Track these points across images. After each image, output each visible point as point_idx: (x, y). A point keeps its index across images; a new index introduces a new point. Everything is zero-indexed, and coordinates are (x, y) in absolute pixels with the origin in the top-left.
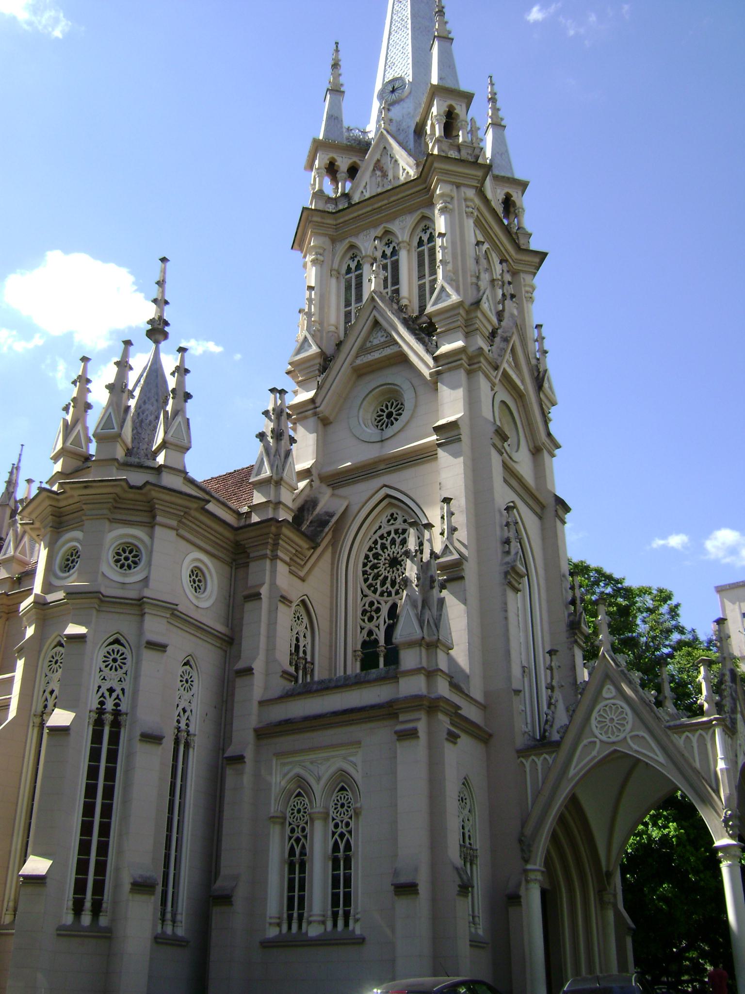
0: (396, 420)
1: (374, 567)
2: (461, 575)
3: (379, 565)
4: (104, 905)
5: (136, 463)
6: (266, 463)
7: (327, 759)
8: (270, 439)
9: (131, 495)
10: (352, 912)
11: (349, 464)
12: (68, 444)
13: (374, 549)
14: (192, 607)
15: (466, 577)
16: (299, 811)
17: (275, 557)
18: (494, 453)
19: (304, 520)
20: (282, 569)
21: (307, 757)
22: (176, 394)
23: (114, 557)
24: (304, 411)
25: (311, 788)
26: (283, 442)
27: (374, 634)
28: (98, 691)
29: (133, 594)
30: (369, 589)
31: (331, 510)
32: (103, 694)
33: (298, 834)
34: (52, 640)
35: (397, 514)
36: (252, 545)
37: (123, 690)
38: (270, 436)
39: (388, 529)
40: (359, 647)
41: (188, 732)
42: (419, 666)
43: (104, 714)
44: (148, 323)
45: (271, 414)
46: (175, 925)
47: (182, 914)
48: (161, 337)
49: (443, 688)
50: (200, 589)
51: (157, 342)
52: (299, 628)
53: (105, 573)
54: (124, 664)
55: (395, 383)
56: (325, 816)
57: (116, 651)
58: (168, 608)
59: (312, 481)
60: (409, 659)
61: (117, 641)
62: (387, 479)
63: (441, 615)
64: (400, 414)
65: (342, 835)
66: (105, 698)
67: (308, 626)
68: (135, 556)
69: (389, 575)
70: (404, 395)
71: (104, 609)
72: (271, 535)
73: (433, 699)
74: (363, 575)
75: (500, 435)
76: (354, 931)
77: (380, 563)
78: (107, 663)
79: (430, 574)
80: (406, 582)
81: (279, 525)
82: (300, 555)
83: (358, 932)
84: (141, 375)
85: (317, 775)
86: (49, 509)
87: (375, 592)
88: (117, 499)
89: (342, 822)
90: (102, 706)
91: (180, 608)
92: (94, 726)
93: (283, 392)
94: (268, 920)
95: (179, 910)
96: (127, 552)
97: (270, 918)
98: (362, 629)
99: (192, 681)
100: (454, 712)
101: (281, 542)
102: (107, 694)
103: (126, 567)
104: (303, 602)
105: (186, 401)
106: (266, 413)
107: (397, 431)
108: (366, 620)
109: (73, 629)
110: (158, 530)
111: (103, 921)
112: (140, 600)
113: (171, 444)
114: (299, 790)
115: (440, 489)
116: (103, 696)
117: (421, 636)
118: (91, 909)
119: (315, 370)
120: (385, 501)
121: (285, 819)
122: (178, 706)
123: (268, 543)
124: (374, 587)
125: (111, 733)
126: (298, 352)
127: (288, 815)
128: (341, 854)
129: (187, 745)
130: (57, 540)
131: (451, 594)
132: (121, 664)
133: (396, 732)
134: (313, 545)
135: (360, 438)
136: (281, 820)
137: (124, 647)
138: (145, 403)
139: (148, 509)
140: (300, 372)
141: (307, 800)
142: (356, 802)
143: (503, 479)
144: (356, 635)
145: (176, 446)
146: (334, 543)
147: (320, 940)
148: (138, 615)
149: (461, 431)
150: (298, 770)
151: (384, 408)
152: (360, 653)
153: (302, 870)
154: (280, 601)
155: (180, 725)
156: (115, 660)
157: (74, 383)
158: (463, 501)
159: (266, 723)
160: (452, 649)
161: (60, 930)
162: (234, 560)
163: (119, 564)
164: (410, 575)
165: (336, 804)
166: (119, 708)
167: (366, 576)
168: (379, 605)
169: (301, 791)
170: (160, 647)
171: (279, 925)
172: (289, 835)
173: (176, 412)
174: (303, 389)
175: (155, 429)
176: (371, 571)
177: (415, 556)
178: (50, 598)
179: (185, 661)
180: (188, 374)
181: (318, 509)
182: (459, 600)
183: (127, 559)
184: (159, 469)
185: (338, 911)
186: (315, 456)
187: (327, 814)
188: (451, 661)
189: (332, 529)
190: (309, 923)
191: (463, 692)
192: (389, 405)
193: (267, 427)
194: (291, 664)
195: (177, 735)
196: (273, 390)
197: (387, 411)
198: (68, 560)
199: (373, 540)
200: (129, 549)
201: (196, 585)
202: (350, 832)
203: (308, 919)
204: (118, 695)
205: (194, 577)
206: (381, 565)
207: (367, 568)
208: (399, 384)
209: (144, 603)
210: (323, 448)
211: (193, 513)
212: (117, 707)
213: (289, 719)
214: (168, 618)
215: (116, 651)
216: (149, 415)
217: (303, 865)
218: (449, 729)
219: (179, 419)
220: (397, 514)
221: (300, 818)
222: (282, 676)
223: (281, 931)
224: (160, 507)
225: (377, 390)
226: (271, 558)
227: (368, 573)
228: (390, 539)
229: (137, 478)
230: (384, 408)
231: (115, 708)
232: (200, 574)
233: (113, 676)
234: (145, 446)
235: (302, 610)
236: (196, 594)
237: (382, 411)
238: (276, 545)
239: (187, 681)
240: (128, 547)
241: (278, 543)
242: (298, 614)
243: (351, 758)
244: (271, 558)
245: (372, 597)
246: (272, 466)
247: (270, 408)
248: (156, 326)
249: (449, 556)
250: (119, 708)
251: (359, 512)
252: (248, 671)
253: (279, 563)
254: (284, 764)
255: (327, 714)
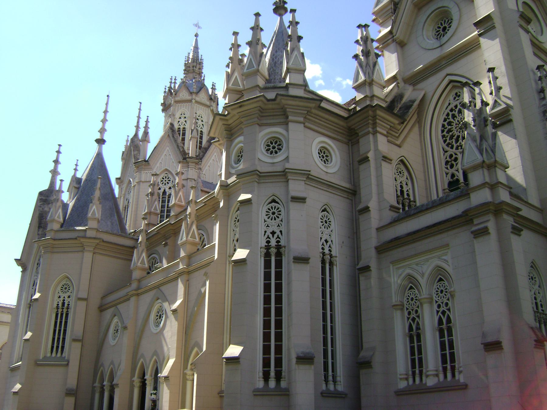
0: (448, 30)
1: (448, 132)
2: (509, 118)
3: (452, 129)
4: (283, 374)
5: (272, 87)
6: (361, 72)
7: (427, 260)
8: (361, 57)
9: (270, 106)
10: (457, 366)
11: (422, 66)
12: (230, 85)
13: (447, 119)
14: (323, 173)
15: (514, 119)
16: (412, 299)
17: (375, 133)
18: (522, 32)
19: (395, 108)
20: (382, 140)
21: (413, 261)
22: (292, 39)
23: (266, 148)
24: (385, 42)
25: (418, 282)
26: (371, 57)
27: (456, 176)
28: (265, 234)
29: (279, 168)
30: (448, 147)
31: (413, 98)
32: (268, 236)
33: (413, 315)
34: (235, 206)
35: (460, 92)
36: (358, 127)
37: (281, 232)
38: (361, 55)
39: (455, 104)
40: (446, 187)
41: (331, 256)
42: (484, 182)
43: (270, 249)
44: (273, 5)
45: (360, 41)
46: (336, 384)
47: (340, 376)
48: (282, 12)
49: (504, 196)
50: (328, 161)
51: (281, 15)
52: (401, 179)
53: (260, 158)
54: (280, 215)
55: (444, 5)
56: (430, 300)
57: (273, 207)
58: (304, 174)
59: (398, 83)
60: (476, 179)
61: (274, 201)
62: (448, 70)
63: (495, 144)
64: (450, 27)
65: (443, 313)
66: (270, 238)
67: (408, 177)
68: (280, 145)
69: (460, 134)
70: (452, 12)
71: (262, 181)
72: (370, 118)
73: (497, 204)
74: (443, 138)
75: (524, 18)
76: (459, 380)
77: (453, 128)
78: (271, 218)
79: (483, 116)
80: (466, 125)
81: (374, 109)
82: (394, 130)
83: (462, 380)
84: (273, 37)
85: (421, 273)
86: (223, 127)
87: (452, 148)
88: (261, 110)
89: (442, 303)
90: (268, 244)
91: (312, 173)
92: (264, 258)
93: (366, 26)
94: (399, 376)
95: (338, 374)
96: (274, 143)
97: (400, 375)
98: (447, 174)
99: (330, 222)
100: (515, 212)
101: (378, 121)
102: (271, 236)
103: (274, 153)
104: (402, 161)
105: (299, 41)
106: (357, 42)
107: (450, 37)
108: (449, 168)
109: (244, 197)
110: (291, 125)
111: (283, 384)
112: (283, 172)
113: (292, 69)
114: (411, 285)
115: (485, 64)
116: (268, 237)
117: (482, 160)
118: (275, 377)
119: (390, 13)
120: (450, 85)
121: (403, 306)
122: (321, 238)
123: (369, 123)
124: (451, 144)
125: (276, 261)
126: (377, 5)
127: (405, 303)
128: (444, 326)
129: (331, 264)
130: (231, 146)
131: (504, 134)
132: (278, 215)
133: (472, 232)
134: (402, 121)
135: (426, 48)
136: (400, 307)
137: (279, 204)
138: (276, 52)
139: (282, 113)
140: (380, 17)
141: (417, 291)
142: (451, 287)
143: (529, 40)
144: (443, 178)
145: (296, 70)
146: (420, 121)
147: (436, 388)
148: (285, 182)
149: (494, 21)
150: (408, 271)
151: (440, 25)
152: (447, 190)
153: (419, 340)
154: (382, 160)
155: (324, 251)
156: (273, 213)
157: (231, 49)
158: (503, 69)
159: (382, 242)
160: (508, 168)
161: (255, 392)
162: (350, 140)
163: (269, 152)
164: (468, 119)
165: (437, 291)
166: (279, 244)
167: (444, 139)
168: (456, 156)
169: (442, 277)
170: (302, 200)
171: (407, 379)
172: (407, 317)
173: (293, 50)
174: (384, 27)
175: (282, 63)
176: (448, 135)
177: (470, 106)
178: (230, 181)
179: (323, 208)
180: (298, 25)
181: (404, 100)
182: (512, 138)
183: (274, 148)
184: (287, 87)
185: (446, 367)
186: (398, 67)
187: (432, 299)
188: (508, 178)
189: (417, 112)
190: (427, 376)
191: (522, 200)
192: (443, 22)
193: (359, 50)
194: (398, 203)
195: (323, 258)
196: (359, 26)
197: (442, 27)
198: (239, 156)
199: (446, 113)
200: (275, 141)
201: (324, 159)
202: (449, 310)
203: (426, 374)
204: (278, 236)
205: (323, 154)
206: (454, 129)
207: (445, 133)
208: (446, 5)
209: (287, 172)
210: (402, 61)
211: (314, 111)
212: (278, 243)
213: (397, 237)
214: (305, 181)
215: (273, 207)
216: (280, 58)
217: (419, 336)
218: (512, 225)
219: (295, 53)
220: (460, 92)
221: (414, 304)
222: (390, 210)
223: (408, 383)
224: (291, 110)
225: (433, 14)
226: (373, 133)
227: (446, 136)
228: (457, 110)
229: (271, 95)
230: (440, 25)
231: (277, 244)
232: (326, 152)
233: (273, 224)
234: (279, 77)
235: (402, 167)
236: (325, 164)
237: (439, 28)
238: (375, 124)
239: (326, 222)
240: (274, 140)
241: (376, 122)
242: (399, 170)
243: (444, 257)
244: (373, 133)
245: (451, 151)
246: (365, 74)
247: (359, 38)
248: (278, 5)
249: (498, 107)
250: (279, 244)
251: (433, 97)
252: (366, 209)
253: (379, 136)
254: (398, 268)
255: (422, 229)
